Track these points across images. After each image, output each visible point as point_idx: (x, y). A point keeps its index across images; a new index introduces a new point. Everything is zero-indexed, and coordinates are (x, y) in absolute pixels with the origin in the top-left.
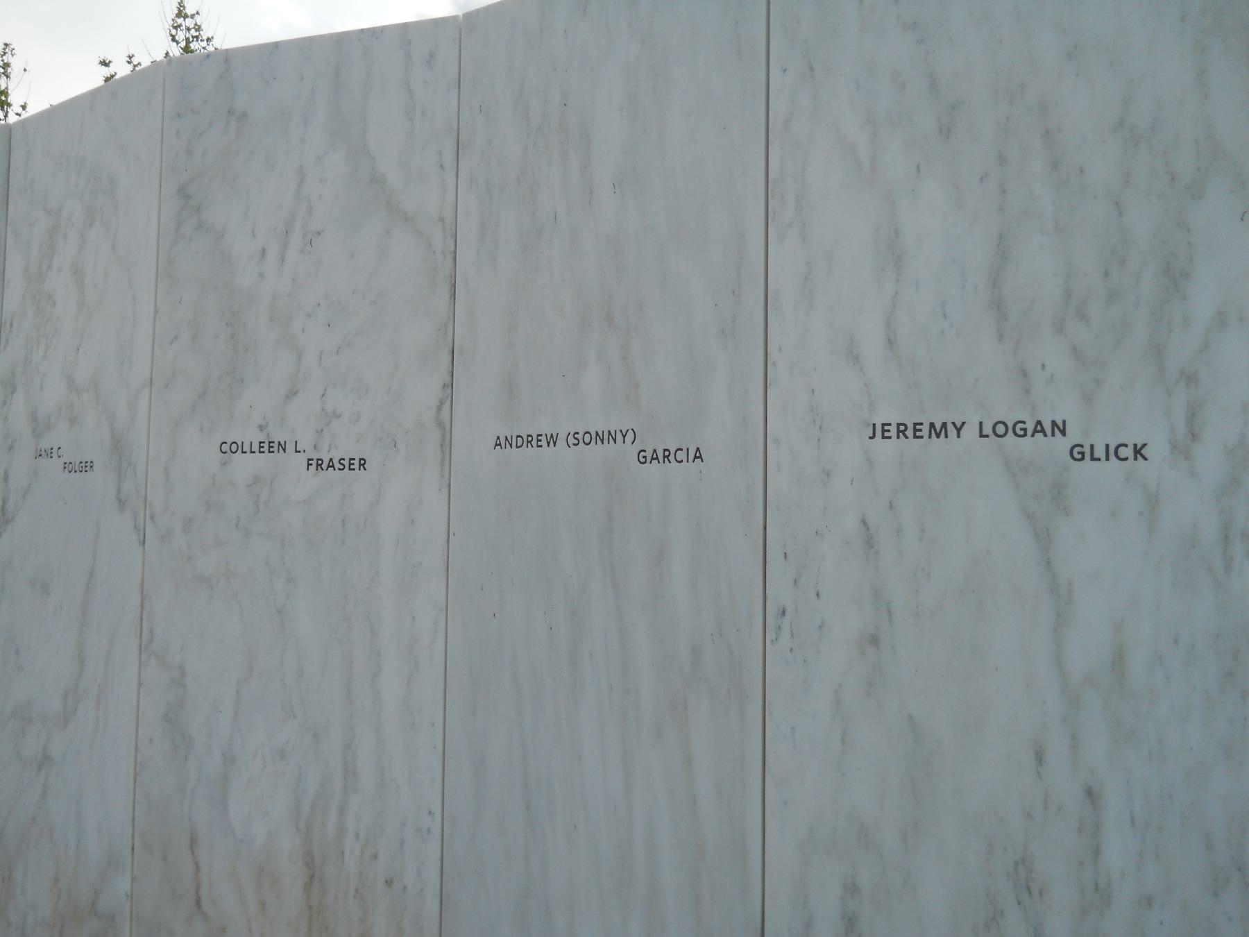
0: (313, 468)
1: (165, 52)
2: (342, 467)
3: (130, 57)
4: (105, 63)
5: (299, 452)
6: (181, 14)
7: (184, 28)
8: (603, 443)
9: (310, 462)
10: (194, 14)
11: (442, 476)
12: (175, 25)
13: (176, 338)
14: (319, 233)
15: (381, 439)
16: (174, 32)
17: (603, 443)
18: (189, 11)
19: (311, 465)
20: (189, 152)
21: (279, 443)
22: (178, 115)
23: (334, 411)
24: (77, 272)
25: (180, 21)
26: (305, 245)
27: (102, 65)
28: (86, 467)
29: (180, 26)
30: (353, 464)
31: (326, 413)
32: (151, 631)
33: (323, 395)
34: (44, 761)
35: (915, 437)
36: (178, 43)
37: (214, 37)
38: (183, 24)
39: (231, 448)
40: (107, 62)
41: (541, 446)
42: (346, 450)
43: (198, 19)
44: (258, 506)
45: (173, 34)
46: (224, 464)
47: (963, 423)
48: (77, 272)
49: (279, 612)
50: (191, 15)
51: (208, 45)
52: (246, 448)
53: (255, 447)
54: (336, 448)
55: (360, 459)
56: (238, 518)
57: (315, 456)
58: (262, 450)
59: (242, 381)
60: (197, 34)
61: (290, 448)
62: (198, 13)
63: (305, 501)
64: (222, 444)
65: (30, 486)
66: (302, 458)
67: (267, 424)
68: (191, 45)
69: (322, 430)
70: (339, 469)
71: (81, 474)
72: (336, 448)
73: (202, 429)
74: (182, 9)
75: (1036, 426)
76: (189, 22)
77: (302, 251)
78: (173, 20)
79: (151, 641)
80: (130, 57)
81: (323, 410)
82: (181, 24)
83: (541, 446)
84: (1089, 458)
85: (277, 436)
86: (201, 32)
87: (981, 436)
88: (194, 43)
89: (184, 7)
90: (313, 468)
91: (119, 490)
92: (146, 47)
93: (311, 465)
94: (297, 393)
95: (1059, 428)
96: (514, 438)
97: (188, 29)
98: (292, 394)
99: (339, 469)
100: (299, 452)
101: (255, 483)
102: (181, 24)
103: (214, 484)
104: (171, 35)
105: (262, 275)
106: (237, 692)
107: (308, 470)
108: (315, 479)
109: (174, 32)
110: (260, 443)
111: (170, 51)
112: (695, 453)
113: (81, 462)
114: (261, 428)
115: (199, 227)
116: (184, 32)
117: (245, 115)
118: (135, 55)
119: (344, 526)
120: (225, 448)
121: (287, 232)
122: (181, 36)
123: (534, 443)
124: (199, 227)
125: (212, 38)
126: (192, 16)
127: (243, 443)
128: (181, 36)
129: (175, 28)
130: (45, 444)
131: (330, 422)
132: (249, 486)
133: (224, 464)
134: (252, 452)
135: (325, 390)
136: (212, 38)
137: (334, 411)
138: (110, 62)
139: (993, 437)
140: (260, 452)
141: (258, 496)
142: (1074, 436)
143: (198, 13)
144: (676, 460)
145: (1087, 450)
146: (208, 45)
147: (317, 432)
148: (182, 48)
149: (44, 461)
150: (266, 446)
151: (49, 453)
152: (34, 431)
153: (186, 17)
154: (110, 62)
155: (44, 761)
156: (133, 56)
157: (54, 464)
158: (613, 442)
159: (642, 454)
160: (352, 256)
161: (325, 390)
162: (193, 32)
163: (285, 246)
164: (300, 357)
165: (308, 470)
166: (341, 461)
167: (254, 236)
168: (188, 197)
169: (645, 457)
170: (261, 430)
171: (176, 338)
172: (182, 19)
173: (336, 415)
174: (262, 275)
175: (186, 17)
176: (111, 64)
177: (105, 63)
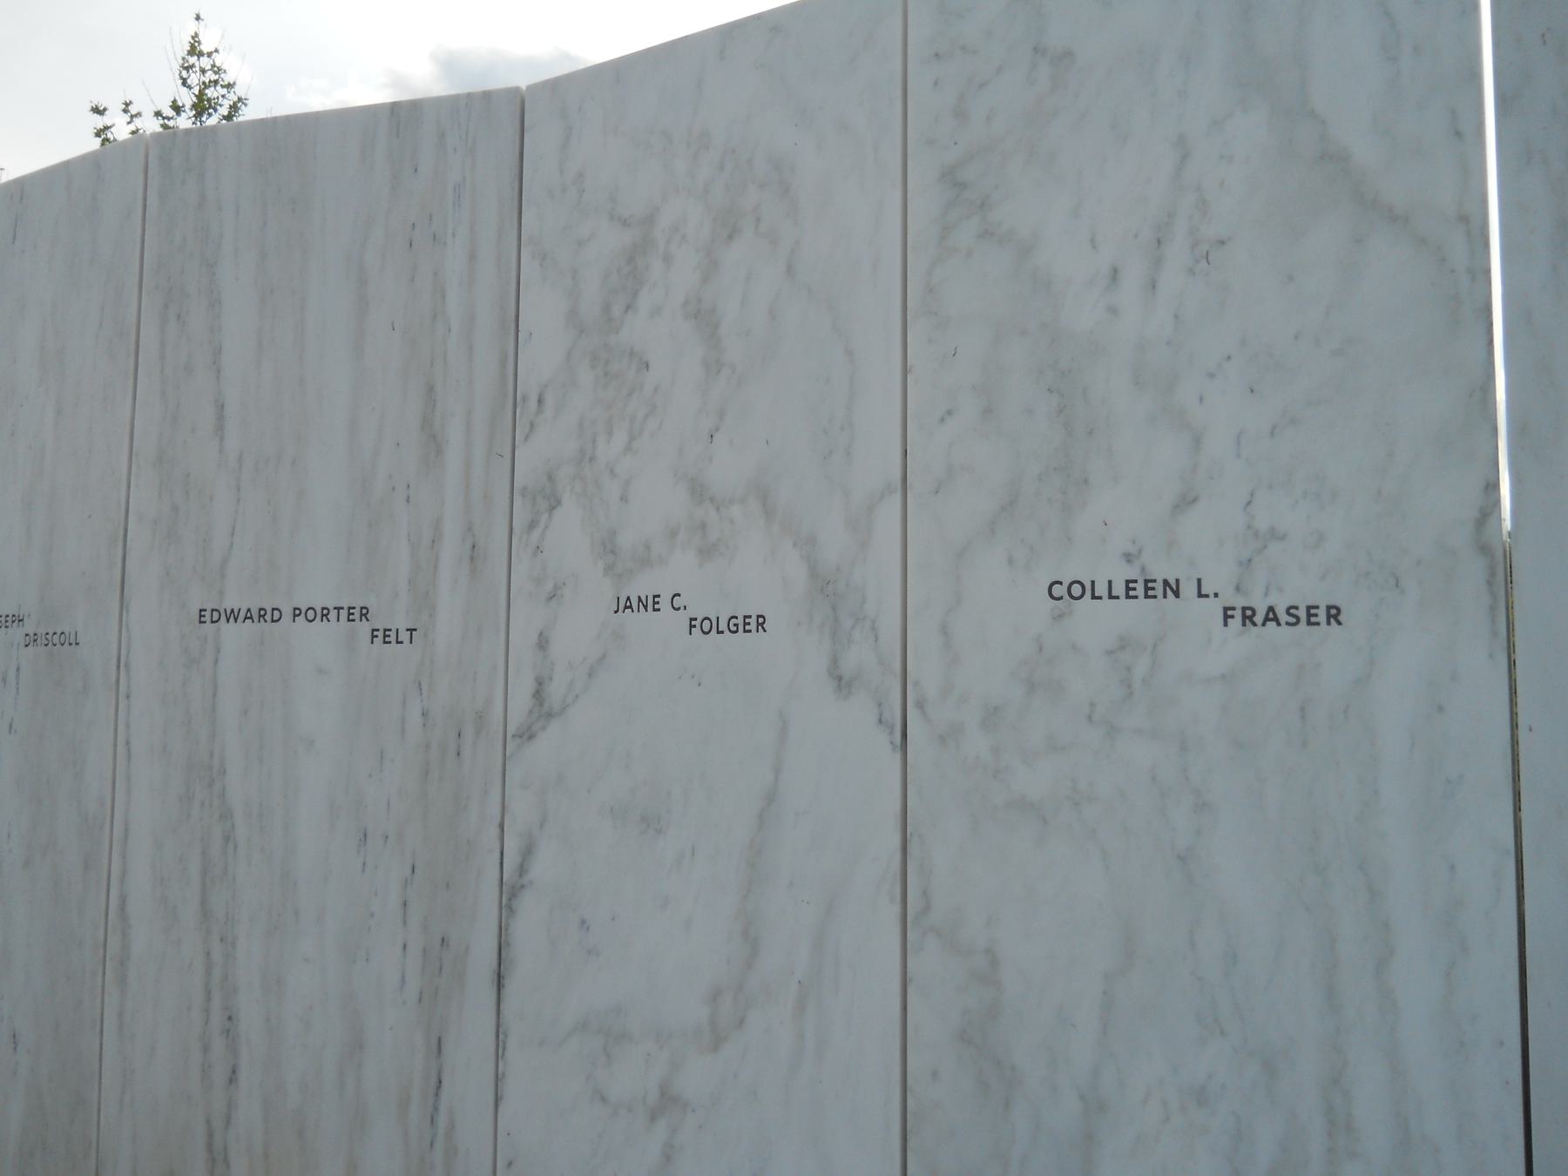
0: (1236, 623)
1: (172, 99)
2: (1293, 620)
3: (127, 105)
4: (97, 111)
5: (1207, 596)
6: (194, 50)
7: (198, 69)
8: (646, 611)
9: (375, 633)
10: (211, 53)
11: (1495, 634)
12: (186, 65)
13: (949, 413)
14: (1223, 243)
15: (1368, 574)
16: (184, 74)
17: (646, 611)
18: (205, 48)
19: (377, 636)
20: (960, 114)
21: (1166, 583)
22: (937, 55)
23: (1272, 529)
24: (703, 317)
25: (193, 60)
26: (1198, 261)
27: (94, 112)
28: (6, 621)
29: (192, 66)
30: (389, 636)
31: (1256, 534)
32: (925, 893)
33: (1249, 503)
34: (667, 1102)
35: (1147, 596)
36: (190, 87)
37: (237, 82)
38: (197, 64)
39: (1081, 590)
40: (101, 108)
41: (659, 610)
42: (1298, 589)
43: (219, 59)
44: (1129, 686)
45: (184, 77)
46: (1058, 617)
47: (408, 630)
48: (703, 317)
49: (1182, 858)
50: (208, 53)
51: (229, 92)
52: (1101, 589)
53: (1119, 589)
54: (1280, 590)
55: (758, 617)
56: (1092, 705)
57: (1239, 602)
58: (351, 617)
59: (1086, 481)
60: (216, 77)
61: (1188, 590)
62: (216, 51)
63: (1223, 676)
64: (674, 596)
65: (604, 657)
66: (1214, 608)
67: (1140, 551)
68: (207, 91)
69: (1250, 560)
70: (1288, 624)
71: (69, 647)
72: (1280, 590)
73: (1011, 561)
74: (196, 44)
75: (1267, 614)
76: (205, 62)
77: (1191, 272)
78: (183, 59)
79: (927, 908)
80: (127, 105)
81: (1249, 527)
82: (193, 64)
83: (659, 610)
84: (1305, 623)
85: (1160, 572)
86: (222, 76)
87: (1200, 595)
88: (212, 89)
89: (199, 42)
90: (1236, 623)
91: (835, 662)
92: (148, 91)
93: (377, 636)
94: (1195, 500)
95: (1171, 589)
96: (269, 613)
97: (203, 71)
98: (1186, 502)
99: (1288, 624)
100: (1207, 596)
101: (1122, 648)
102: (193, 64)
103: (1041, 650)
104: (181, 78)
105: (1113, 311)
106: (1105, 993)
107: (372, 643)
108: (1237, 642)
109: (184, 74)
110: (1128, 582)
111: (177, 98)
112: (1264, 612)
113: (47, 634)
114: (1128, 558)
115: (985, 234)
116: (198, 74)
117: (1068, 55)
118: (133, 101)
119: (1303, 717)
120: (1057, 590)
121: (1159, 241)
122: (194, 79)
123: (268, 617)
124: (985, 234)
125: (234, 83)
126: (209, 55)
127: (1093, 582)
128: (194, 79)
129: (187, 69)
130: (640, 587)
131: (1265, 547)
132: (1110, 653)
133: (1058, 617)
134: (1111, 597)
135: (1252, 495)
136: (234, 83)
137: (1272, 529)
138: (105, 109)
139: (727, 632)
140: (1128, 597)
141: (1129, 669)
142: (364, 628)
143: (216, 51)
144: (729, 629)
145: (1088, 587)
146: (229, 92)
147: (1240, 564)
148: (196, 96)
149: (636, 620)
150: (1140, 587)
151: (651, 603)
152: (609, 568)
153: (201, 54)
154: (105, 109)
155: (667, 1102)
156: (131, 102)
157: (668, 623)
158: (226, 621)
159: (733, 621)
160: (1291, 279)
161: (1252, 495)
162: (210, 76)
163: (1158, 263)
164: (1197, 442)
165: (372, 643)
166: (1292, 611)
167: (1094, 247)
168: (962, 186)
169: (736, 625)
170: (1128, 561)
171: (949, 413)
172: (196, 57)
173: (1275, 535)
174: (1113, 311)
175: (201, 54)
176: (107, 112)
177: (97, 111)
